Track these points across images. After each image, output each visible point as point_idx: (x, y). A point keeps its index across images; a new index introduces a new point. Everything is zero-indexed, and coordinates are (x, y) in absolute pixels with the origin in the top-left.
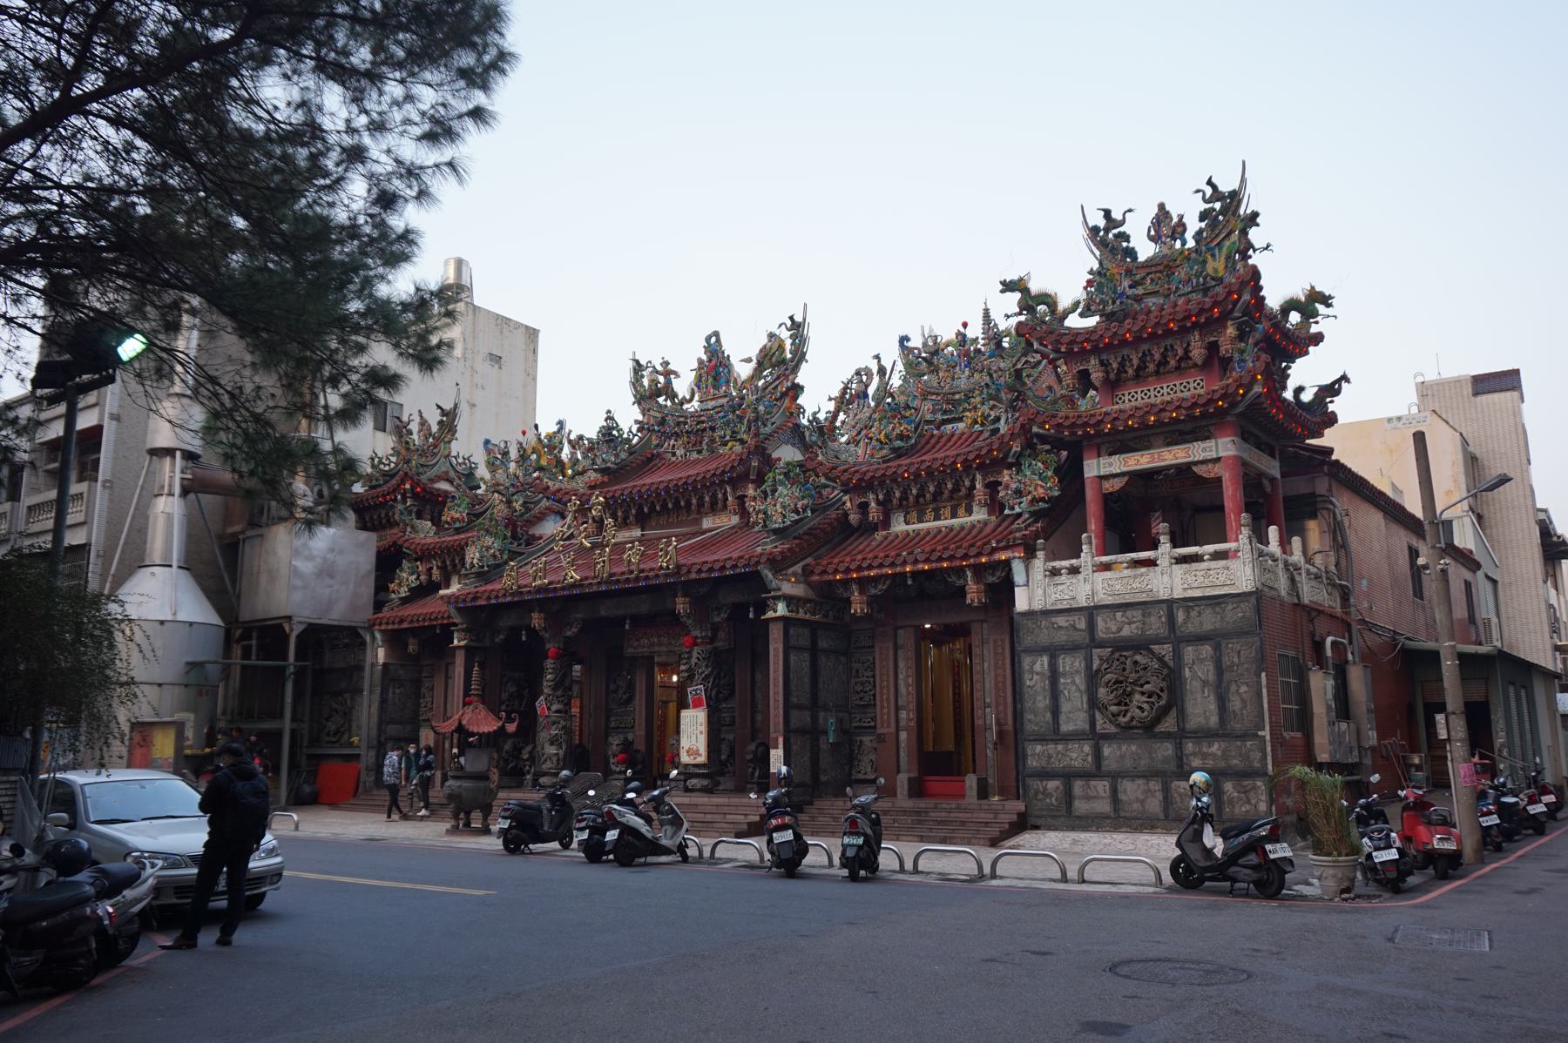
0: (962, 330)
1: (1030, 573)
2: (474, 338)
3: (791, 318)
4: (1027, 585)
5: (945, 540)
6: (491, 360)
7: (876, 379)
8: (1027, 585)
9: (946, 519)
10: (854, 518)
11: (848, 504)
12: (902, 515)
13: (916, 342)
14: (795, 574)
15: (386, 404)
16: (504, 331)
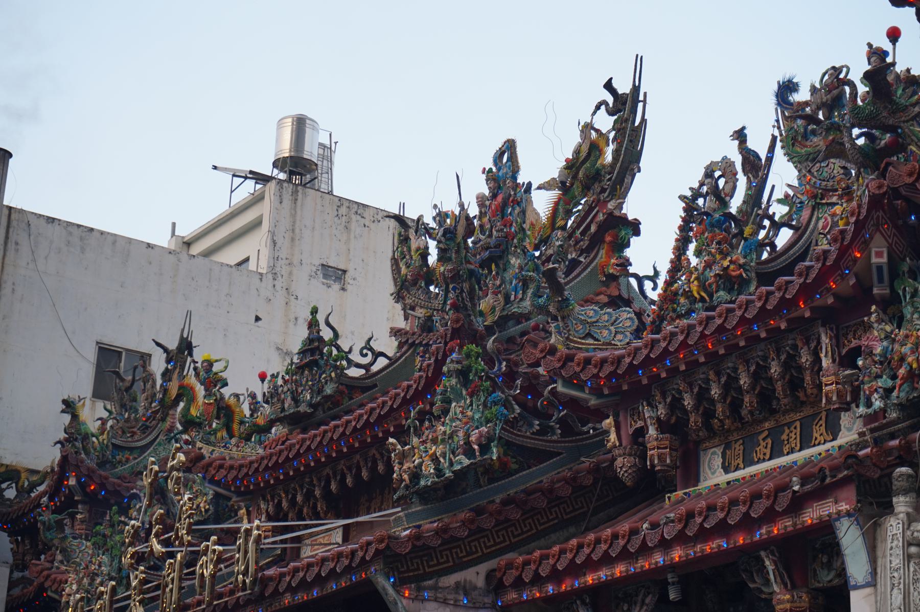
0: (887, 45)
1: (879, 553)
2: (293, 240)
3: (609, 86)
4: (872, 583)
5: (906, 527)
6: (326, 276)
7: (742, 182)
8: (872, 583)
9: (792, 451)
10: (623, 465)
11: (613, 437)
12: (719, 451)
13: (795, 80)
14: (464, 588)
15: (120, 353)
16: (353, 225)
